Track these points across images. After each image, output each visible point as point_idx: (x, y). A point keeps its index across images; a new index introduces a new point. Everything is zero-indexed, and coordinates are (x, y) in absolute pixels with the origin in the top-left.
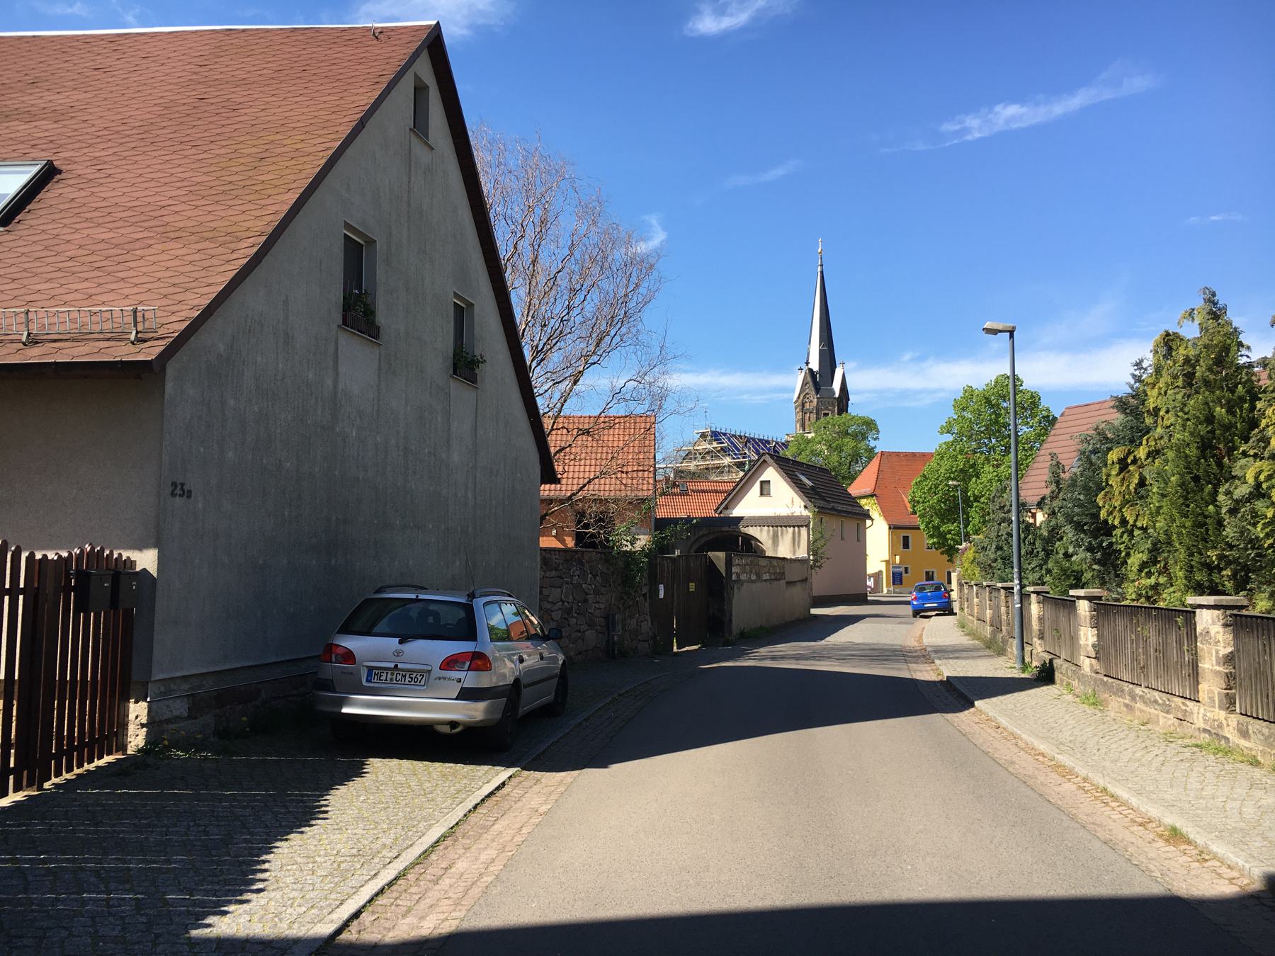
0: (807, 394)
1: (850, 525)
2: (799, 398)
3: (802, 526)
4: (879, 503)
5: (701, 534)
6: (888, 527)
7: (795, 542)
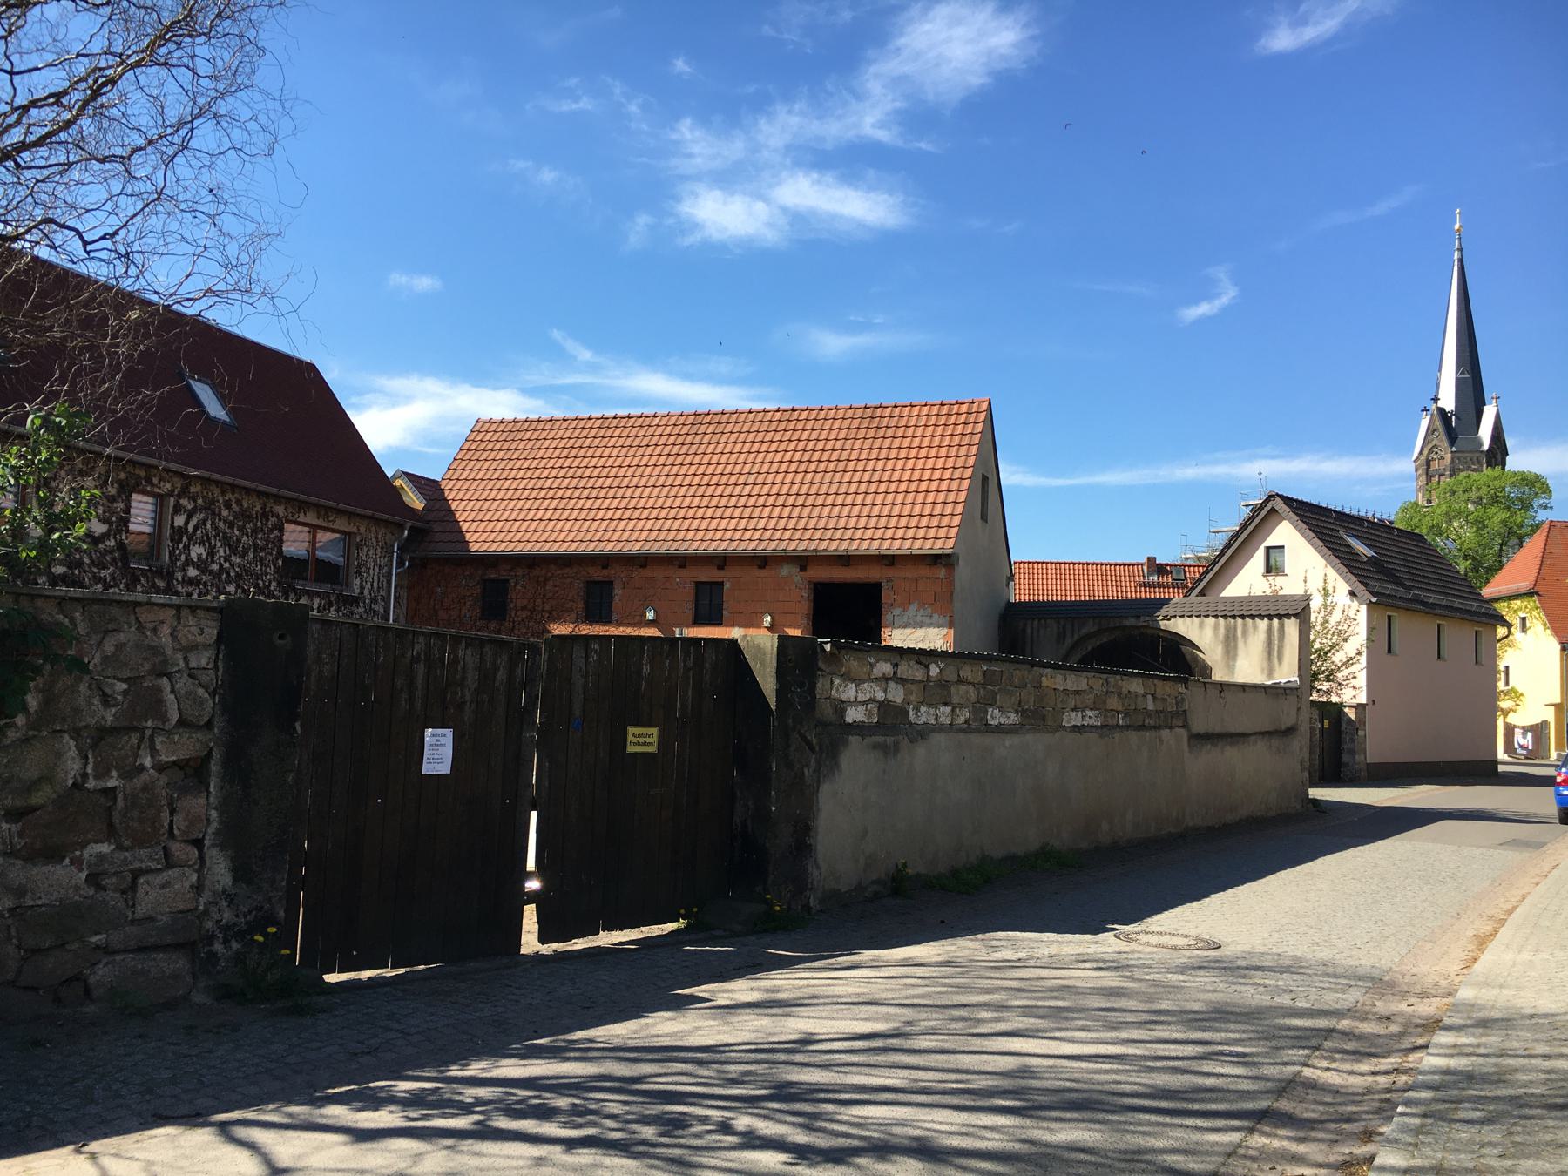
0: (1435, 446)
1: (1459, 636)
2: (1421, 453)
3: (1288, 616)
4: (1544, 607)
5: (1084, 631)
6: (1558, 647)
7: (1272, 650)
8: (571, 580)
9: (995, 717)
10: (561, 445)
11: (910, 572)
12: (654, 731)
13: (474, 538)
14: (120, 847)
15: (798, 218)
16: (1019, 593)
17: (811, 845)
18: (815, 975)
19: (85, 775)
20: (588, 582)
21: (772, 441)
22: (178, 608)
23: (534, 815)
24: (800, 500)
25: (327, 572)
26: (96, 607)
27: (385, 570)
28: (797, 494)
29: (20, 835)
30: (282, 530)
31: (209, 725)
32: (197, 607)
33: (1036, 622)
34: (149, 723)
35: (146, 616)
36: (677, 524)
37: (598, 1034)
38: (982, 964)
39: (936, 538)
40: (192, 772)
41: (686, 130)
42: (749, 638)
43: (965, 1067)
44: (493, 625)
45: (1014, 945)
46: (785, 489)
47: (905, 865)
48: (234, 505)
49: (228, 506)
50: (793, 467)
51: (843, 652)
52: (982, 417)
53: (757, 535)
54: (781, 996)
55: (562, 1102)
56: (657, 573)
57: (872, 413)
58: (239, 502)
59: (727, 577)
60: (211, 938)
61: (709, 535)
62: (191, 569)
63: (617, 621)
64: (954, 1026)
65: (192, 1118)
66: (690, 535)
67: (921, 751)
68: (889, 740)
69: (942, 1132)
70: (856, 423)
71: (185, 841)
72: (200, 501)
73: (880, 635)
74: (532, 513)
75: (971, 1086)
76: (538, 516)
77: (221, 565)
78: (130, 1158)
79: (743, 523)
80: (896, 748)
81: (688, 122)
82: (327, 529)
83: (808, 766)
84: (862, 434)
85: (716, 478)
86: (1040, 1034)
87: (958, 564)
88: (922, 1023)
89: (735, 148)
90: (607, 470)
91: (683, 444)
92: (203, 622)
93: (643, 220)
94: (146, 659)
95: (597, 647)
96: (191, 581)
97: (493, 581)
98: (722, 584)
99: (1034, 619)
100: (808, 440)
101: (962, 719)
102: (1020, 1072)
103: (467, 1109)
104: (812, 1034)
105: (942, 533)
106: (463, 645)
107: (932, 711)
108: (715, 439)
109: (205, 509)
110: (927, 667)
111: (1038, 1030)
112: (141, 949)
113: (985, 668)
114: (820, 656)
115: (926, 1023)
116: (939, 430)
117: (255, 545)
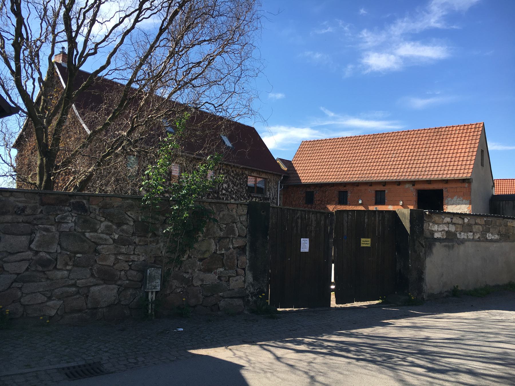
8: (333, 191)
9: (489, 236)
10: (329, 148)
11: (454, 185)
12: (369, 240)
13: (303, 179)
14: (225, 270)
15: (406, 59)
16: (497, 191)
17: (423, 278)
18: (428, 320)
19: (216, 250)
20: (339, 191)
21: (401, 142)
22: (237, 204)
23: (333, 265)
24: (412, 162)
25: (260, 190)
26: (218, 204)
27: (276, 189)
28: (411, 160)
29: (202, 265)
30: (247, 178)
31: (246, 237)
32: (242, 204)
33: (504, 202)
34: (231, 236)
35: (230, 207)
36: (368, 172)
37: (360, 331)
38: (488, 320)
39: (464, 173)
40: (242, 250)
41: (365, 34)
42: (400, 210)
43: (484, 350)
44: (309, 206)
45: (501, 314)
46: (406, 158)
47: (457, 286)
48: (234, 172)
49: (233, 172)
50: (409, 150)
51: (433, 214)
52: (481, 129)
53: (397, 174)
54: (417, 325)
55: (352, 348)
56: (363, 188)
57: (438, 131)
58: (235, 171)
59: (386, 189)
60: (248, 296)
61: (380, 175)
62: (223, 191)
63: (349, 204)
64: (479, 338)
65: (252, 342)
66: (373, 175)
67: (462, 248)
68: (450, 244)
69: (477, 368)
70: (432, 134)
71: (241, 269)
72: (225, 171)
73: (443, 207)
74: (321, 170)
75: (486, 356)
76: (323, 171)
77: (231, 189)
78: (240, 351)
79: (391, 171)
80: (453, 246)
81: (365, 30)
82: (259, 177)
83: (422, 252)
84: (434, 138)
85: (380, 152)
86: (511, 343)
87: (472, 182)
88: (467, 337)
89: (383, 37)
90: (344, 155)
91: (370, 145)
92: (244, 208)
93: (350, 67)
94: (230, 218)
95: (350, 213)
96: (224, 194)
97: (309, 192)
98: (385, 191)
99: (503, 201)
100: (414, 141)
101: (477, 237)
102: (504, 353)
103: (326, 347)
104: (429, 337)
105: (466, 171)
106: (311, 213)
107: (466, 234)
108: (381, 142)
109: (227, 173)
110: (463, 219)
111: (510, 342)
112: (231, 298)
113: (485, 219)
114: (424, 216)
115: (469, 337)
116: (464, 135)
117: (240, 183)
